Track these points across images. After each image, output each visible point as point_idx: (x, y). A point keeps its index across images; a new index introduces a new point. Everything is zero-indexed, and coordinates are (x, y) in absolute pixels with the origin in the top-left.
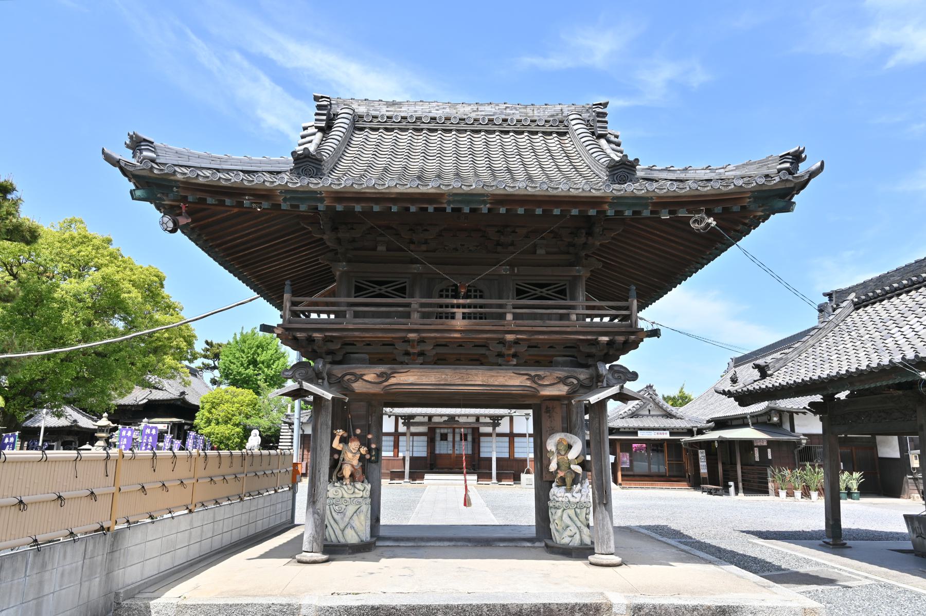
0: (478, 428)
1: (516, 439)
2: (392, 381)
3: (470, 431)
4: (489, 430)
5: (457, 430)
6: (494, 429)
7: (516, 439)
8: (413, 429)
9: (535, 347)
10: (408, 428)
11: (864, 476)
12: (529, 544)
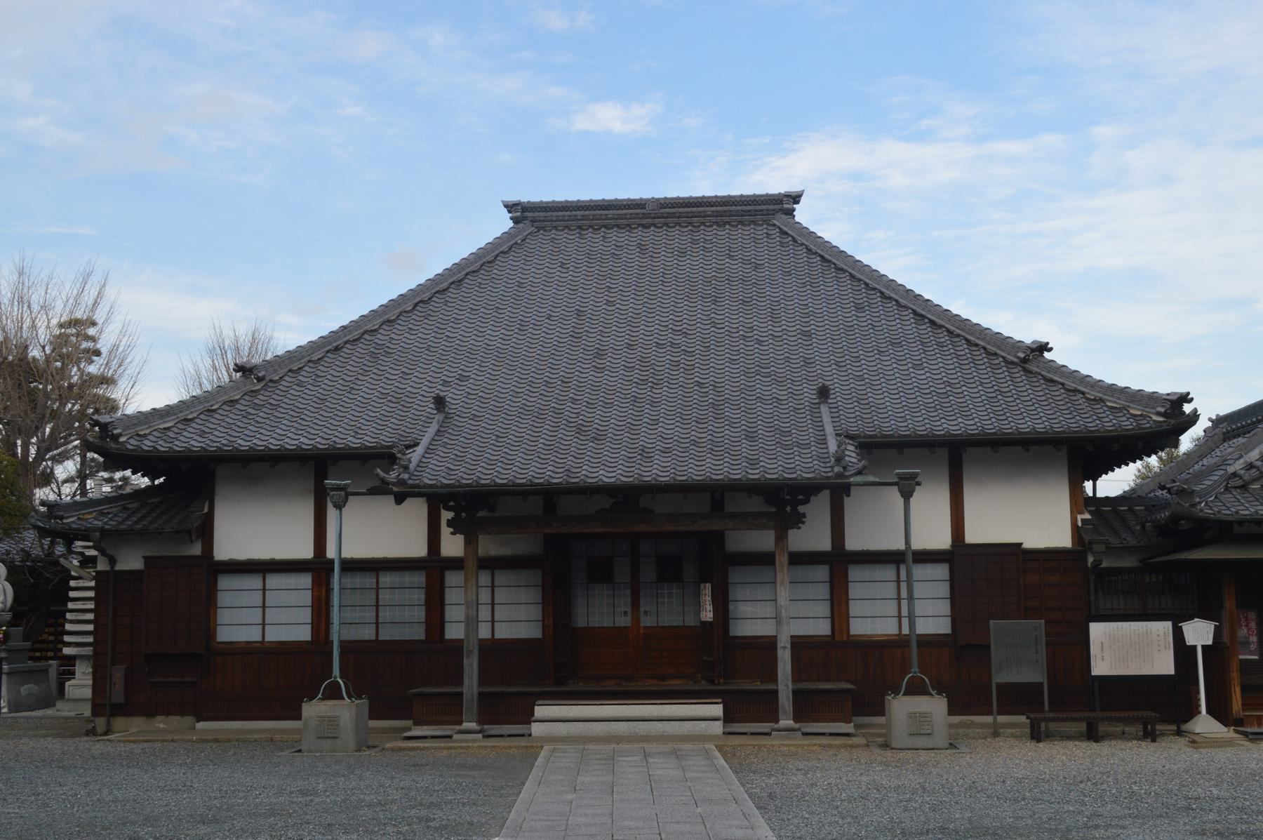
0: (720, 536)
1: (855, 573)
4: (763, 540)
6: (781, 538)
7: (855, 573)
8: (489, 546)
9: (89, 275)
10: (470, 542)
11: (371, 699)
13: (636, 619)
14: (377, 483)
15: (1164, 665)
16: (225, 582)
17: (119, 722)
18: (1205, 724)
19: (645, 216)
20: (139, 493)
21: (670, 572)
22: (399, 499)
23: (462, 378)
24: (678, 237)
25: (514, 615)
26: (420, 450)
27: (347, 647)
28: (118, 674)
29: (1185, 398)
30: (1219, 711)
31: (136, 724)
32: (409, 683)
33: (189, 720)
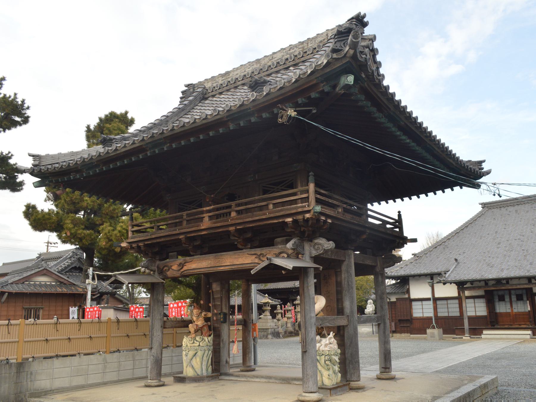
3: (524, 291)
5: (513, 292)
7: (414, 303)
12: (266, 380)
13: (512, 310)
14: (438, 281)
16: (414, 303)
17: (395, 335)
19: (518, 202)
20: (394, 284)
21: (520, 298)
22: (444, 284)
23: (464, 253)
24: (527, 207)
25: (477, 309)
26: (449, 272)
27: (470, 318)
28: (393, 324)
31: (398, 335)
32: (452, 327)
33: (409, 334)
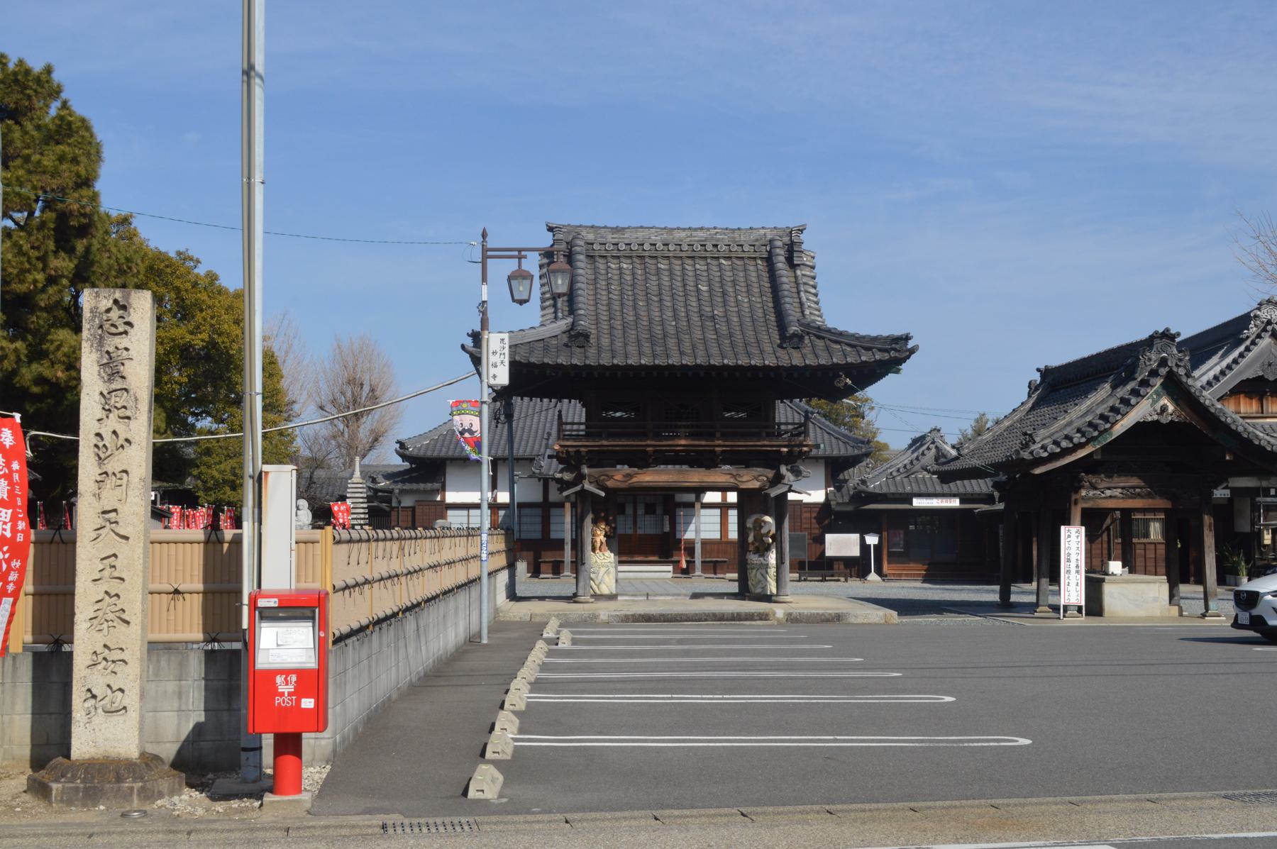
2: (634, 480)
13: (635, 531)
15: (856, 552)
18: (873, 576)
29: (907, 338)
30: (879, 571)
